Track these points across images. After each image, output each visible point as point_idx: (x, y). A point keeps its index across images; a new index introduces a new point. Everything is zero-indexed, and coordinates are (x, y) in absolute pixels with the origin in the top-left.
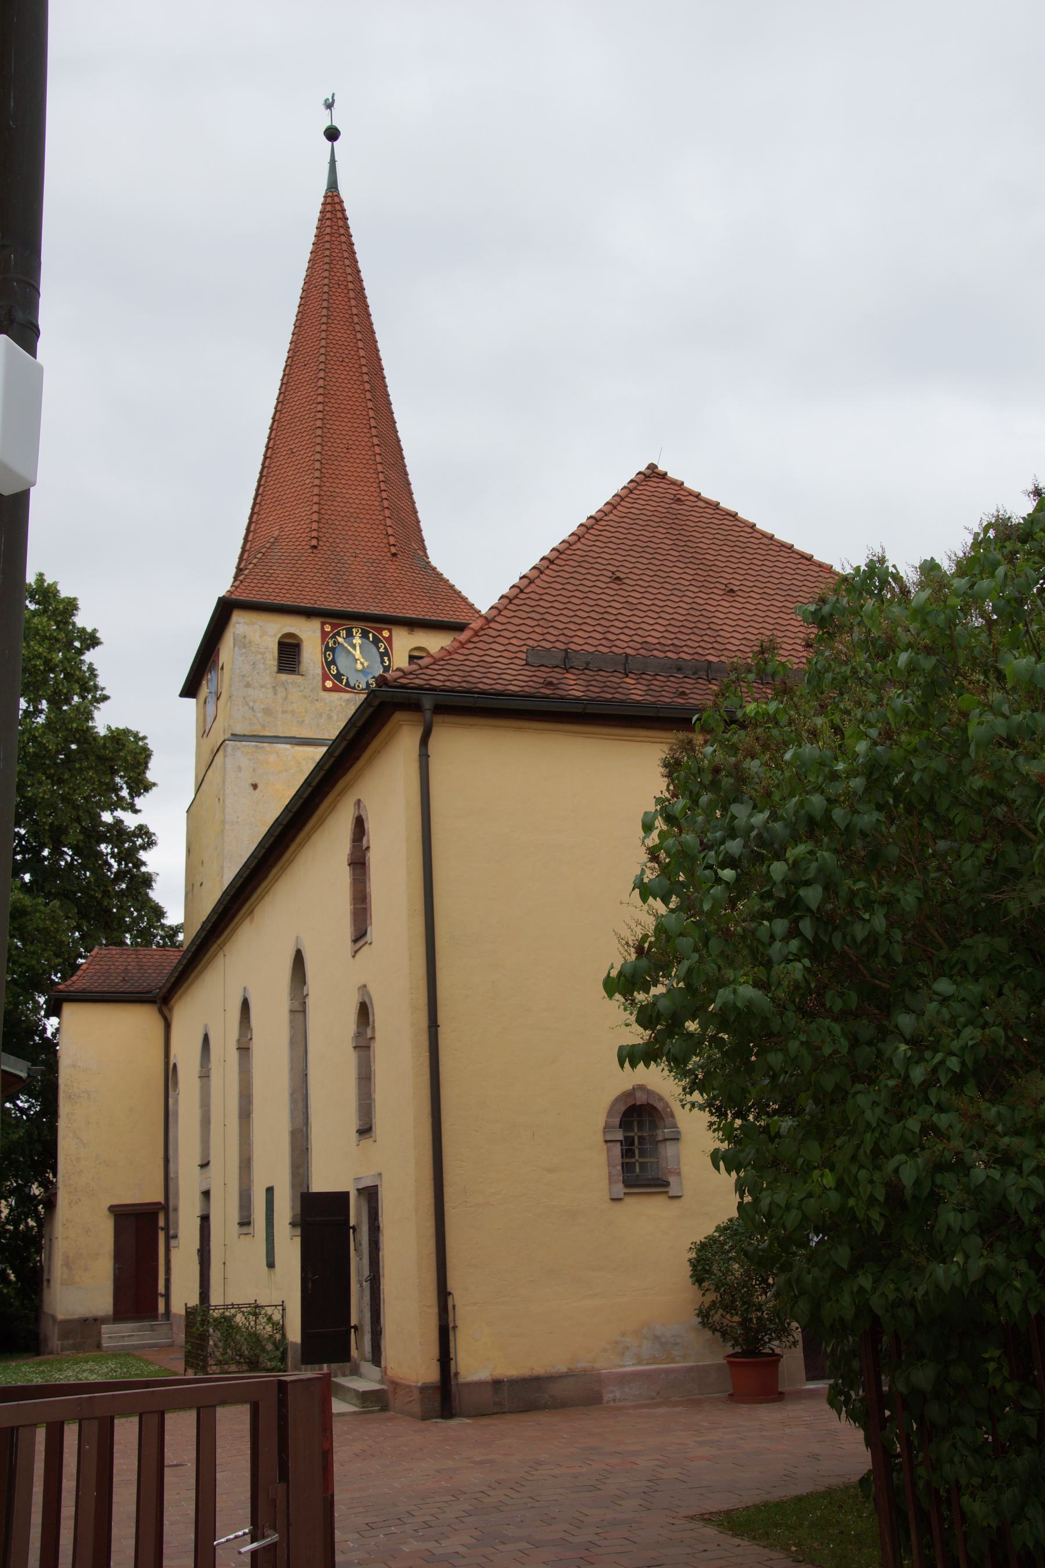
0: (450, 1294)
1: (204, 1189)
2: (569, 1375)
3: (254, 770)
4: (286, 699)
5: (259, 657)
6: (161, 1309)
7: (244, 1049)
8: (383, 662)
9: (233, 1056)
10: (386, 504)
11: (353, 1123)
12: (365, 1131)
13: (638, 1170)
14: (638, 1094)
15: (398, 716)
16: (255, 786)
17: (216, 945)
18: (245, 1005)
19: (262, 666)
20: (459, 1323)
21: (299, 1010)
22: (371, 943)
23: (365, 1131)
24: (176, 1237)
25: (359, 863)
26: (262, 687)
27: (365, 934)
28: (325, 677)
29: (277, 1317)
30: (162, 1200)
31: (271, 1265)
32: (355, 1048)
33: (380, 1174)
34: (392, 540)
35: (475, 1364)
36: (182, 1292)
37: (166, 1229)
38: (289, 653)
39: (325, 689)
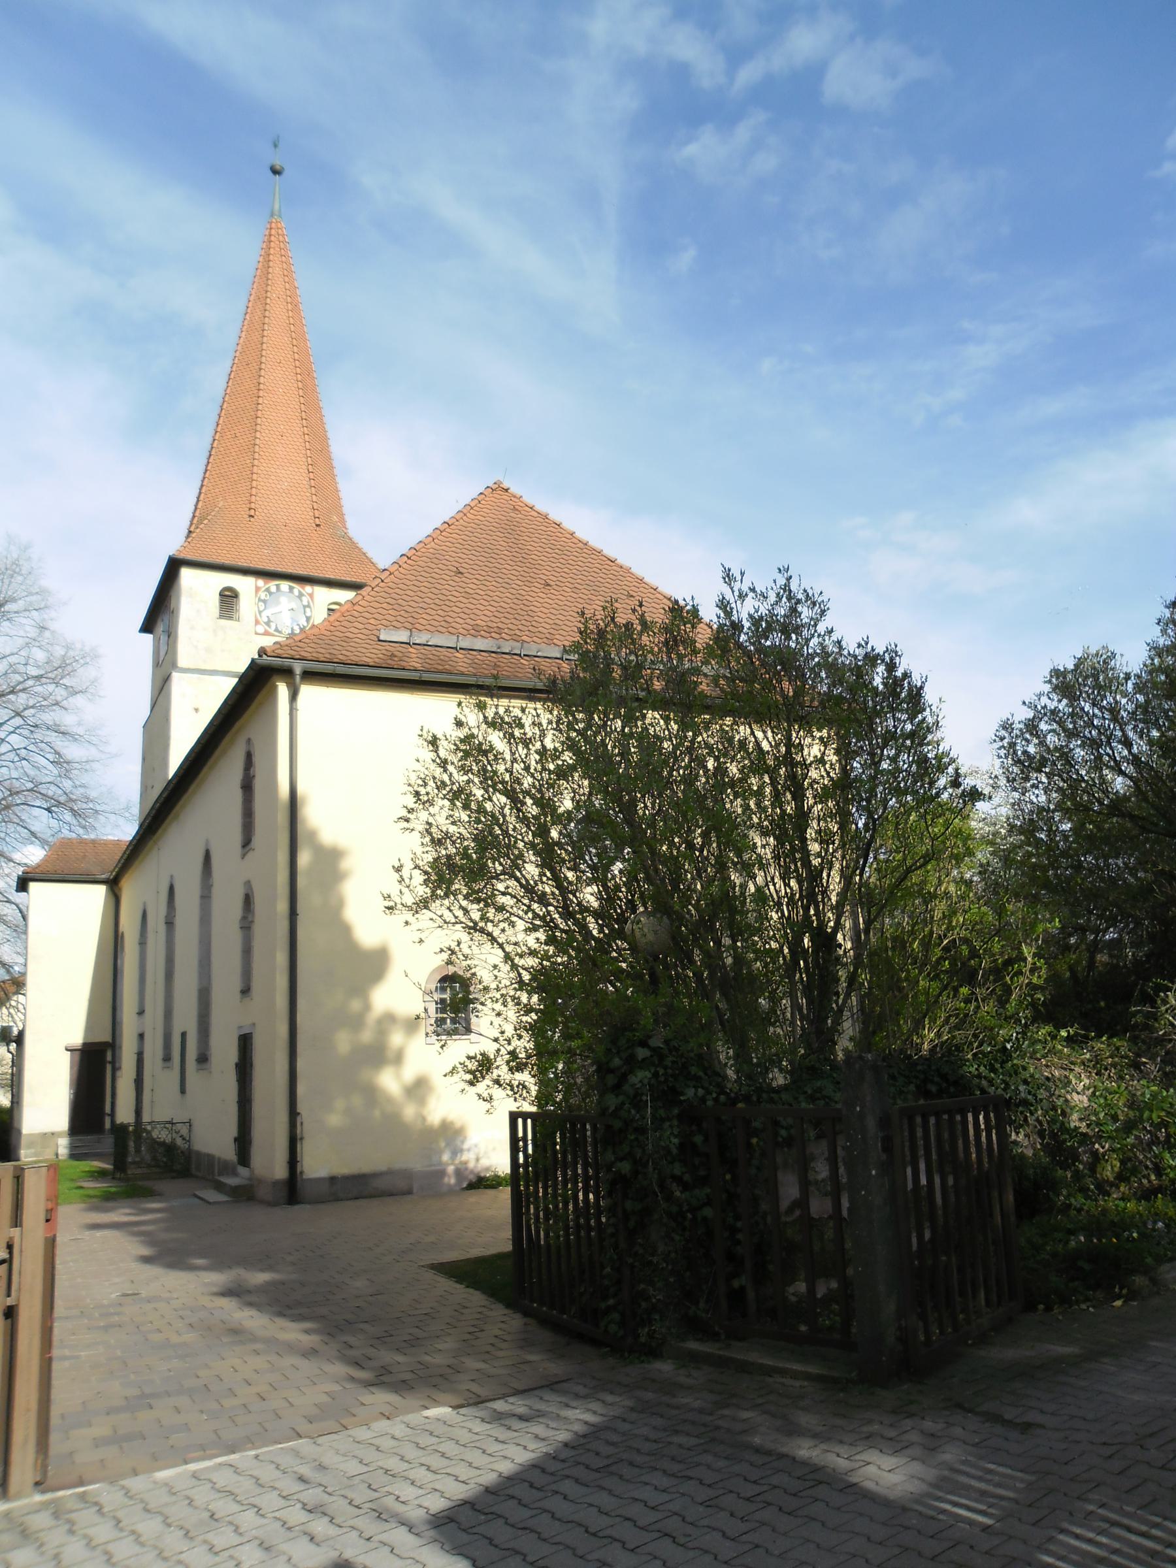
2: (390, 1173)
7: (170, 924)
9: (162, 928)
11: (237, 985)
12: (246, 991)
15: (275, 677)
18: (171, 889)
20: (305, 1135)
21: (206, 896)
23: (246, 991)
24: (120, 1068)
25: (247, 787)
28: (257, 622)
29: (184, 1131)
31: (183, 1091)
37: (113, 1062)
38: (229, 598)
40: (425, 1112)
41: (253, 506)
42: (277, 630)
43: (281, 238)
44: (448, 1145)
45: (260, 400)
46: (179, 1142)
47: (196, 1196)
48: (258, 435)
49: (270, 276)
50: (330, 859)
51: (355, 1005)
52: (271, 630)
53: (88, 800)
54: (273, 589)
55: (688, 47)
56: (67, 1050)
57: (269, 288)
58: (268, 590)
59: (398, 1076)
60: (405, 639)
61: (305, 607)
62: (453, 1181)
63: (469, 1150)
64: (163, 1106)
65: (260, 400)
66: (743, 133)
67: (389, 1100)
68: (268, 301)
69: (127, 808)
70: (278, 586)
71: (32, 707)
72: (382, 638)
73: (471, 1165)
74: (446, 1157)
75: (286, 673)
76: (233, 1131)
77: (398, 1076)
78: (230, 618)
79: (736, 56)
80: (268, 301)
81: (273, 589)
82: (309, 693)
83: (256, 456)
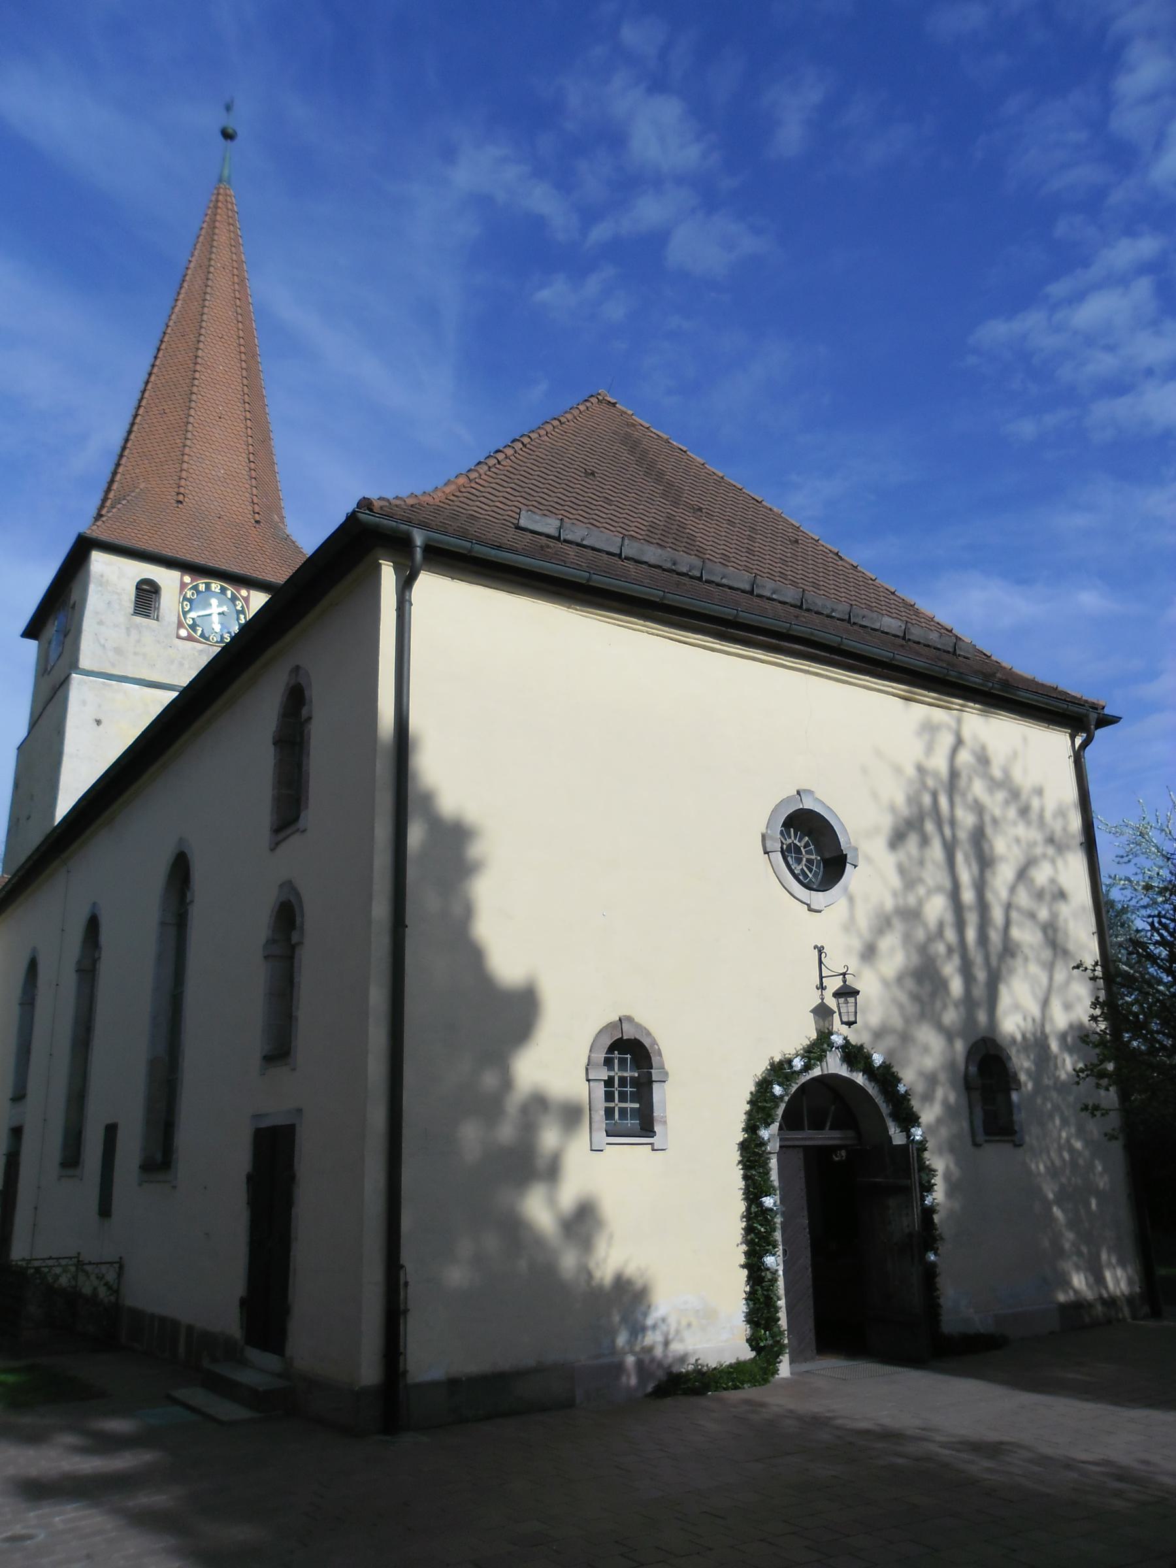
0: (402, 1267)
2: (539, 1370)
3: (100, 706)
4: (139, 641)
8: (238, 619)
9: (70, 979)
10: (253, 474)
11: (253, 1039)
12: (279, 1051)
14: (625, 1026)
20: (411, 1305)
22: (304, 831)
23: (279, 1051)
25: (292, 741)
27: (296, 819)
28: (180, 625)
29: (111, 1276)
32: (266, 957)
33: (299, 1111)
34: (257, 509)
35: (430, 1358)
38: (147, 595)
39: (179, 637)
40: (592, 1265)
42: (202, 635)
43: (230, 206)
44: (624, 1320)
45: (197, 375)
46: (102, 1292)
47: (175, 1401)
48: (192, 412)
49: (215, 244)
50: (454, 838)
51: (489, 1080)
52: (197, 636)
54: (202, 587)
55: (542, 200)
57: (213, 256)
58: (195, 588)
59: (552, 1201)
60: (552, 531)
61: (239, 612)
62: (633, 1381)
63: (654, 1327)
65: (197, 375)
66: (593, 284)
67: (538, 1241)
68: (212, 269)
70: (208, 586)
72: (523, 523)
73: (659, 1352)
74: (621, 1340)
75: (397, 545)
77: (552, 1201)
78: (148, 616)
79: (589, 216)
80: (212, 269)
81: (202, 587)
83: (189, 435)
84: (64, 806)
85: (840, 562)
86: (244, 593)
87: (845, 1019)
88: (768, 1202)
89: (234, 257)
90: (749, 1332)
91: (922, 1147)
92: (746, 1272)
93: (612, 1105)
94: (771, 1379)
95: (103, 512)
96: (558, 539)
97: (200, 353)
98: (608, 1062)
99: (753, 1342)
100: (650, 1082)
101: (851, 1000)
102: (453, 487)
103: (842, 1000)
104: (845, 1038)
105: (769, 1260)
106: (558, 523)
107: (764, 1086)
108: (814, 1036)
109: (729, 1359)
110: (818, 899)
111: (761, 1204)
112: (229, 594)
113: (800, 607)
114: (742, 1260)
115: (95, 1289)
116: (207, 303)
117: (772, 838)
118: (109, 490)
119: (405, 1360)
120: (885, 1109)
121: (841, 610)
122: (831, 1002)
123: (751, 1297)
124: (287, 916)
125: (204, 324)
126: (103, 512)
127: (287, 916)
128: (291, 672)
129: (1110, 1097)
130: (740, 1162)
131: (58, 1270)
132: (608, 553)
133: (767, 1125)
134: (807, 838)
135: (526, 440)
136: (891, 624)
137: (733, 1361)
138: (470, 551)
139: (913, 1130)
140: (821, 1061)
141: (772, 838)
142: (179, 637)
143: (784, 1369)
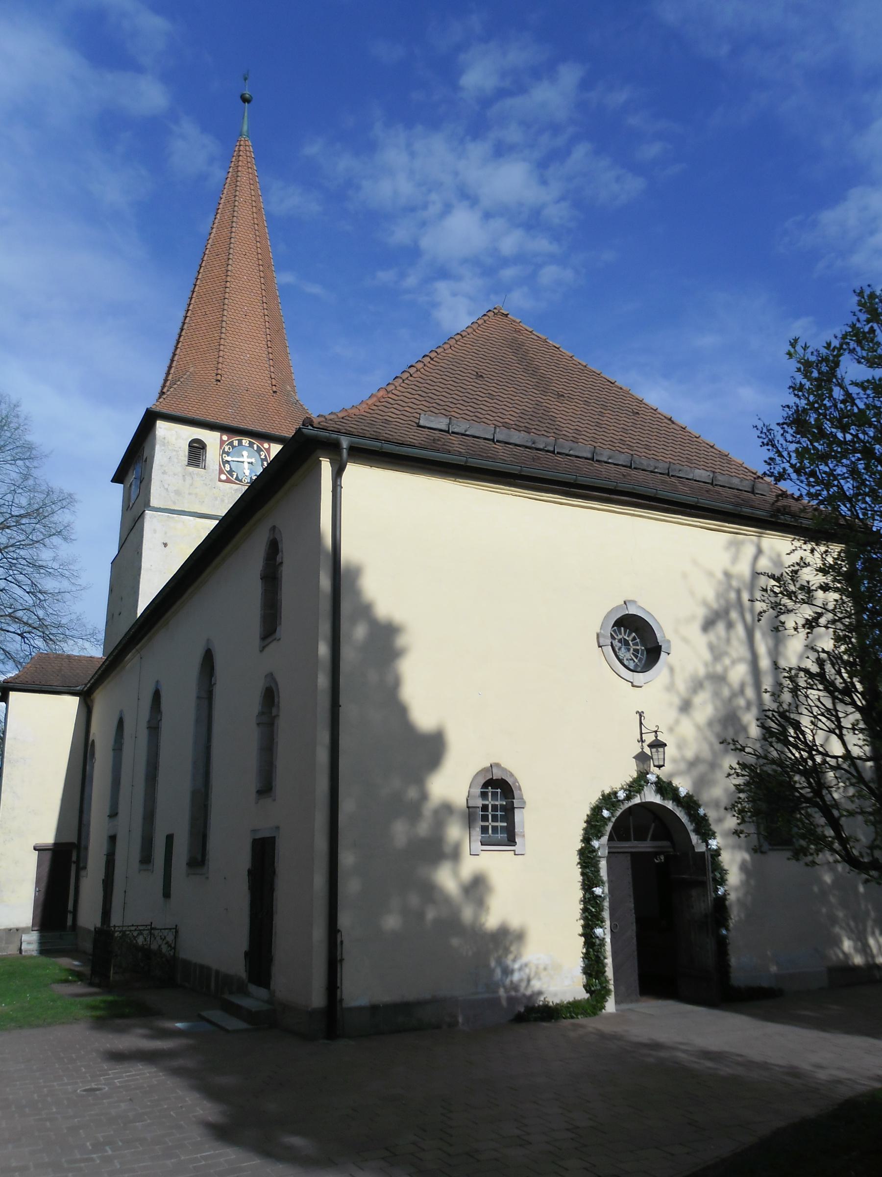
0: (339, 931)
1: (112, 833)
2: (435, 1001)
3: (166, 533)
4: (192, 485)
5: (175, 453)
6: (69, 922)
9: (143, 734)
11: (251, 782)
12: (266, 789)
13: (490, 831)
14: (495, 770)
16: (165, 545)
17: (134, 651)
19: (176, 460)
20: (344, 956)
23: (266, 789)
24: (85, 868)
25: (271, 577)
26: (175, 474)
28: (221, 472)
29: (170, 938)
30: (75, 841)
32: (258, 724)
33: (278, 828)
36: (89, 916)
37: (77, 862)
38: (197, 450)
39: (220, 480)
41: (219, 372)
42: (237, 478)
46: (164, 948)
48: (225, 313)
53: (59, 626)
54: (236, 443)
56: (35, 849)
60: (443, 427)
64: (138, 907)
68: (237, 204)
69: (93, 634)
70: (240, 442)
71: (12, 546)
72: (422, 423)
75: (331, 448)
76: (243, 944)
78: (197, 466)
80: (237, 204)
81: (236, 443)
82: (354, 472)
83: (224, 330)
84: (143, 603)
85: (673, 426)
86: (266, 445)
87: (656, 764)
88: (598, 891)
89: (253, 193)
90: (585, 980)
91: (717, 853)
92: (583, 939)
93: (487, 824)
94: (599, 1012)
95: (165, 390)
96: (448, 432)
97: (230, 268)
98: (484, 795)
99: (587, 987)
100: (513, 809)
101: (661, 750)
102: (375, 399)
103: (654, 750)
104: (658, 777)
105: (599, 931)
106: (448, 421)
107: (596, 810)
108: (635, 775)
109: (568, 998)
110: (639, 678)
111: (593, 892)
112: (255, 446)
113: (630, 467)
114: (580, 930)
115: (160, 946)
116: (234, 230)
117: (604, 637)
118: (168, 374)
119: (341, 992)
120: (690, 827)
121: (662, 467)
122: (647, 750)
123: (586, 956)
124: (270, 697)
125: (232, 246)
126: (165, 390)
127: (270, 697)
128: (270, 530)
129: (751, 829)
130: (579, 863)
131: (135, 934)
132: (485, 439)
133: (598, 838)
134: (634, 634)
135: (433, 355)
136: (702, 474)
137: (571, 1000)
138: (381, 448)
139: (710, 841)
140: (640, 793)
141: (604, 637)
142: (220, 480)
143: (610, 1006)
